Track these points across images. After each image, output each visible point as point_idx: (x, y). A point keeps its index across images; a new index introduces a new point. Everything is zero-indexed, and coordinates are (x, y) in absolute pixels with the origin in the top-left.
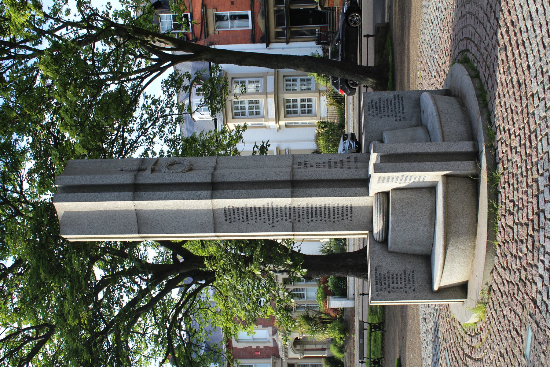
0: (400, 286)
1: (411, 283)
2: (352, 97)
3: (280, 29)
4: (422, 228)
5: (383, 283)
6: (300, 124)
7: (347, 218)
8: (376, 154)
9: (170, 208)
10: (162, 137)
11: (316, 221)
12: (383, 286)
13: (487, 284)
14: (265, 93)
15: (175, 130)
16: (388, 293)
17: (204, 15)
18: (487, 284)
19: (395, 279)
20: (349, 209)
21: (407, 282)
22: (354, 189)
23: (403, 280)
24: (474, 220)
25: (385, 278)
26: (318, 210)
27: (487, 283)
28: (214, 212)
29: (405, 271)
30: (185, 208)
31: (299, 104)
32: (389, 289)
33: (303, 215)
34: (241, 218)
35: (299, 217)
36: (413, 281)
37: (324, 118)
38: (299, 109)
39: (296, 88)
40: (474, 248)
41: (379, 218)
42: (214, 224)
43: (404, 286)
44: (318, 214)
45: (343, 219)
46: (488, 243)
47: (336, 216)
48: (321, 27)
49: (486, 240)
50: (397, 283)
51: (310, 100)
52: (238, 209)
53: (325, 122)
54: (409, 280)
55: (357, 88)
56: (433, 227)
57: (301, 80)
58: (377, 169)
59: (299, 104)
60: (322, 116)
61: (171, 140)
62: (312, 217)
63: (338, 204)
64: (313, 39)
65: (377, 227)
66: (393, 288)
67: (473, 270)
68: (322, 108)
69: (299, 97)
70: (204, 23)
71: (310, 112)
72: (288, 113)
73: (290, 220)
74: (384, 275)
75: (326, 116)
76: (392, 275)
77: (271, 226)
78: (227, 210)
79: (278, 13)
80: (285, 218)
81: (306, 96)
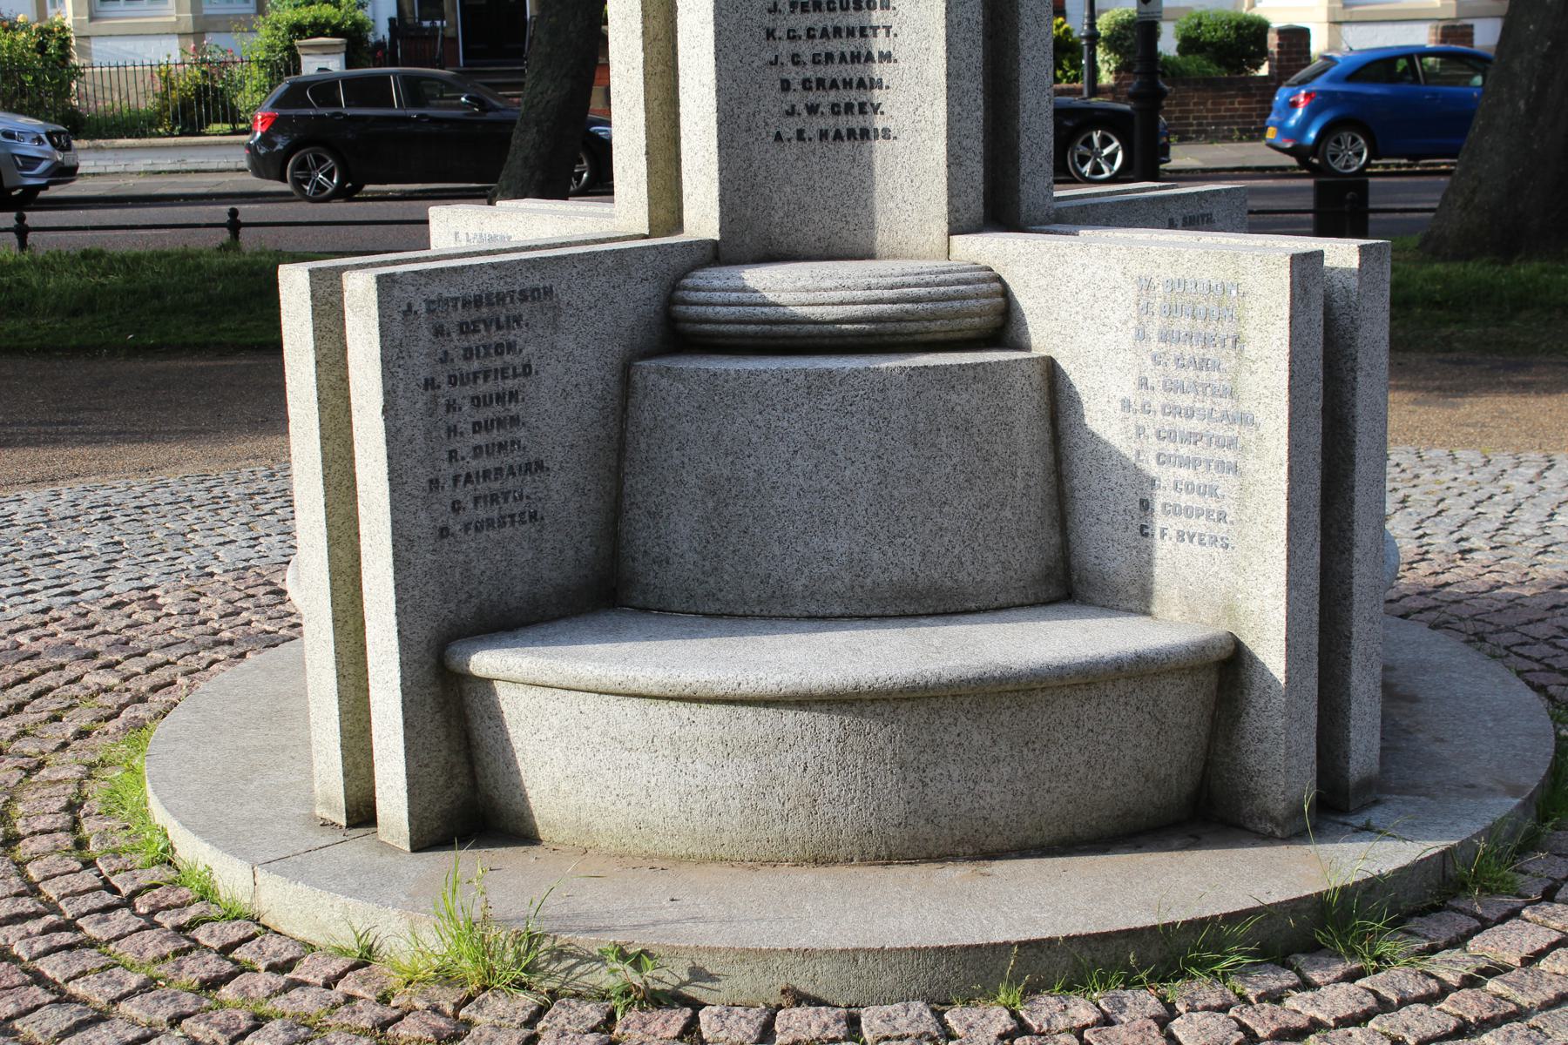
0: (463, 447)
1: (482, 513)
2: (245, 164)
4: (839, 547)
5: (474, 339)
7: (791, 112)
12: (457, 343)
13: (698, 974)
16: (424, 374)
19: (494, 411)
20: (856, 121)
21: (483, 487)
22: (980, 148)
23: (490, 463)
24: (995, 842)
25: (499, 349)
27: (711, 978)
29: (540, 465)
32: (442, 379)
36: (490, 523)
37: (84, 52)
40: (818, 861)
41: (860, 295)
45: (786, 86)
46: (1007, 945)
47: (806, 49)
48: (455, 40)
49: (1013, 937)
50: (477, 427)
53: (65, 57)
54: (494, 498)
56: (855, 608)
58: (1305, 268)
60: (96, 46)
63: (886, 57)
64: (407, 8)
65: (785, 287)
66: (451, 407)
67: (659, 863)
74: (511, 347)
75: (96, 60)
76: (513, 396)
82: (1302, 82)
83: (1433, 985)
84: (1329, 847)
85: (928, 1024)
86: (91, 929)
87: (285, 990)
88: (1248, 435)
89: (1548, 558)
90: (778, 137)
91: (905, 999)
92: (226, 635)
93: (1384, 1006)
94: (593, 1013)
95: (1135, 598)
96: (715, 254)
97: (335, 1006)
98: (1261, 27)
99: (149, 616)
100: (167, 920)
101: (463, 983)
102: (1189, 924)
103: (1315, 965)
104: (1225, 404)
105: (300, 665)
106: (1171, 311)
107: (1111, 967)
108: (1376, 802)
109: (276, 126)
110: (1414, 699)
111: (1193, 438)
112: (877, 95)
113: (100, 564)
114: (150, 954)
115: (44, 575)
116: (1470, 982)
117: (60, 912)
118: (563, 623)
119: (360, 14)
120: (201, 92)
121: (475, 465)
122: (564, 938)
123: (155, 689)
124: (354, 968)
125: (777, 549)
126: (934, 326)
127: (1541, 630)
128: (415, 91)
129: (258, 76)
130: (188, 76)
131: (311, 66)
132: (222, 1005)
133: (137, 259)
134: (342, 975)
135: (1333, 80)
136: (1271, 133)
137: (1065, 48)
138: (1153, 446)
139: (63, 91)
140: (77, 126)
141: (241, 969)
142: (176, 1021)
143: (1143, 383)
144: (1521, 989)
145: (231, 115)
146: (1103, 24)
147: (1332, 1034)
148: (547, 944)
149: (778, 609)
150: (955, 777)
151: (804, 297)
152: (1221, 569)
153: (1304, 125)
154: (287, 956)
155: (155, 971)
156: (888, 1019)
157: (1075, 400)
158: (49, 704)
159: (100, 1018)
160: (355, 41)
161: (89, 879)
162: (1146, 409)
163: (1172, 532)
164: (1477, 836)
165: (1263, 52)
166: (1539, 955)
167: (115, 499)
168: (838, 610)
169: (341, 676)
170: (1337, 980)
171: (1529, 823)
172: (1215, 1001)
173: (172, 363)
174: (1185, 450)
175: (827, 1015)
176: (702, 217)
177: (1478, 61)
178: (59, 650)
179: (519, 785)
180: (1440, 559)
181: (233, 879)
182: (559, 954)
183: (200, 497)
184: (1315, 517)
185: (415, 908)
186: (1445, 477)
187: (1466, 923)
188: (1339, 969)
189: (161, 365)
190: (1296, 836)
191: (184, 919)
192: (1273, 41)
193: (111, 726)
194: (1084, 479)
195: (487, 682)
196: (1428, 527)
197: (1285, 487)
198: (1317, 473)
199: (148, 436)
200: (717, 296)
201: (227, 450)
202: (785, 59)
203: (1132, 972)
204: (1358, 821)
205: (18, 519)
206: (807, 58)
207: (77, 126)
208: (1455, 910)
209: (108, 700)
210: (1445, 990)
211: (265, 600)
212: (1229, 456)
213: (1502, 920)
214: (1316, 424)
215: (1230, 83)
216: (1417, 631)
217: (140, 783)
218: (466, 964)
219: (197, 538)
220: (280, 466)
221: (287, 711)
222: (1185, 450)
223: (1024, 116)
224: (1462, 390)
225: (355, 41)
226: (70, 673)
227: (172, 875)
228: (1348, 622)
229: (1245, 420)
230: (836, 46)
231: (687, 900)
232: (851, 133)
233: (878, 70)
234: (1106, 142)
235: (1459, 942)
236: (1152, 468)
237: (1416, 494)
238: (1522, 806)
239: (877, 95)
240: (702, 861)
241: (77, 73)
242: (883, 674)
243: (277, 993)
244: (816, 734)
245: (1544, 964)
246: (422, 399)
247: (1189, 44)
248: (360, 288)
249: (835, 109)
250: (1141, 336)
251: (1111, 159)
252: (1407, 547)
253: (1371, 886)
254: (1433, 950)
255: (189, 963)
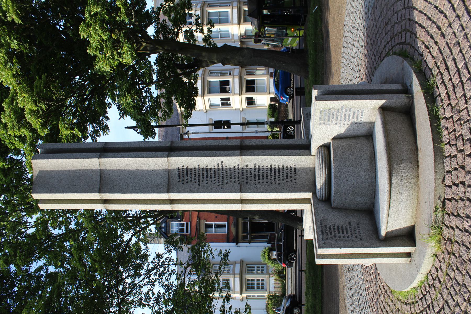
1: (358, 233)
3: (245, 234)
4: (363, 174)
5: (329, 233)
6: (256, 297)
7: (292, 181)
8: (317, 91)
9: (130, 168)
10: (160, 282)
11: (263, 183)
12: (329, 236)
13: (439, 198)
14: (234, 274)
15: (170, 279)
16: (334, 242)
17: (198, 223)
18: (439, 198)
19: (340, 230)
20: (293, 170)
21: (353, 232)
22: (297, 151)
23: (349, 231)
24: (414, 147)
25: (330, 229)
26: (265, 171)
27: (440, 196)
28: (169, 172)
29: (349, 223)
30: (144, 168)
31: (256, 282)
32: (335, 238)
33: (251, 177)
34: (193, 179)
35: (247, 179)
36: (359, 231)
37: (272, 293)
38: (256, 286)
39: (254, 272)
41: (321, 170)
42: (168, 185)
43: (350, 236)
44: (265, 176)
45: (287, 181)
46: (434, 146)
47: (282, 178)
50: (343, 233)
51: (263, 280)
52: (191, 169)
53: (273, 296)
54: (355, 231)
55: (294, 262)
57: (258, 267)
58: (317, 99)
59: (256, 282)
60: (271, 291)
61: (166, 285)
62: (259, 179)
63: (283, 165)
65: (320, 182)
66: (340, 237)
67: (418, 204)
68: (271, 286)
69: (255, 277)
70: (198, 228)
71: (263, 288)
72: (248, 289)
73: (238, 182)
76: (338, 227)
77: (220, 187)
78: (181, 171)
79: (244, 224)
80: (234, 180)
81: (260, 277)
82: (279, 98)
83: (439, 74)
84: (414, 92)
85: (448, 159)
86: (429, 302)
87: (441, 270)
88: (345, 107)
89: (360, 57)
90: (296, 183)
91: (443, 163)
92: (374, 276)
93: (443, 82)
94: (446, 217)
95: (372, 125)
96: (314, 193)
97: (445, 261)
98: (270, 105)
99: (371, 289)
100: (428, 289)
101: (440, 239)
102: (429, 115)
103: (436, 94)
104: (340, 111)
105: (380, 264)
106: (324, 120)
107: (437, 128)
108: (406, 84)
109: (284, 263)
110: (387, 78)
111: (345, 116)
112: (289, 167)
113: (361, 296)
114: (434, 292)
115: (362, 306)
116: (438, 68)
117: (426, 307)
118: (376, 220)
119: (267, 249)
120: (279, 275)
121: (349, 234)
122: (433, 221)
123: (384, 289)
124: (437, 258)
125: (364, 184)
126: (327, 158)
127: (373, 58)
128: (279, 240)
129: (276, 265)
130: (276, 277)
131: (275, 257)
132: (444, 281)
133: (307, 287)
134: (439, 260)
135: (279, 93)
136: (287, 103)
137: (274, 136)
138: (346, 122)
139: (278, 296)
140: (284, 295)
141: (437, 277)
142: (447, 289)
143: (336, 124)
144: (439, 59)
145: (282, 270)
146: (269, 130)
147: (449, 91)
148: (434, 224)
149: (374, 184)
150: (404, 153)
151: (322, 179)
152: (367, 110)
153: (286, 98)
154: (435, 269)
155: (438, 292)
156: (447, 166)
157: (339, 135)
158: (387, 307)
159: (447, 302)
160: (271, 250)
161: (420, 302)
162: (340, 123)
163: (361, 119)
164: (412, 68)
165: (274, 105)
166: (433, 57)
167: (349, 293)
168: (374, 174)
169: (385, 257)
170: (438, 90)
171: (409, 59)
172: (443, 110)
173: (325, 282)
174: (347, 117)
175: (446, 176)
176: (308, 195)
177: (276, 71)
178: (377, 304)
179: (405, 228)
180: (361, 75)
181: (420, 277)
182: (435, 222)
183: (349, 279)
184: (358, 96)
185: (427, 246)
186: (346, 74)
187: (427, 69)
188: (436, 90)
189: (325, 284)
190: (412, 97)
191: (428, 286)
192: (272, 103)
193: (391, 296)
194: (352, 133)
195: (386, 233)
196: (355, 76)
197: (353, 101)
198: (351, 96)
199: (338, 287)
200: (321, 193)
201: (340, 274)
202: (283, 182)
203: (438, 124)
204: (409, 87)
205: (352, 309)
206: (283, 178)
207: (284, 295)
208: (425, 70)
209: (386, 297)
210: (440, 72)
211: (368, 269)
212: (348, 110)
213: (427, 63)
214: (343, 96)
215: (279, 110)
216: (374, 78)
217: (402, 292)
218: (437, 238)
219: (356, 280)
220: (343, 266)
221: (389, 266)
222: (347, 117)
223: (292, 143)
224: (331, 72)
225: (271, 250)
226: (381, 303)
227: (419, 288)
228: (375, 90)
229: (342, 108)
230: (281, 174)
231: (425, 200)
232: (295, 171)
233: (285, 167)
234: (289, 129)
235: (431, 70)
236: (350, 122)
237: (349, 78)
238: (406, 60)
239: (289, 167)
240: (418, 197)
241: (275, 294)
242: (386, 167)
243: (442, 271)
244: (396, 178)
245: (434, 56)
246: (338, 242)
247: (273, 116)
248: (320, 251)
249: (291, 174)
250: (328, 124)
251: (291, 128)
252: (359, 80)
253: (421, 85)
254: (432, 74)
255: (436, 286)
